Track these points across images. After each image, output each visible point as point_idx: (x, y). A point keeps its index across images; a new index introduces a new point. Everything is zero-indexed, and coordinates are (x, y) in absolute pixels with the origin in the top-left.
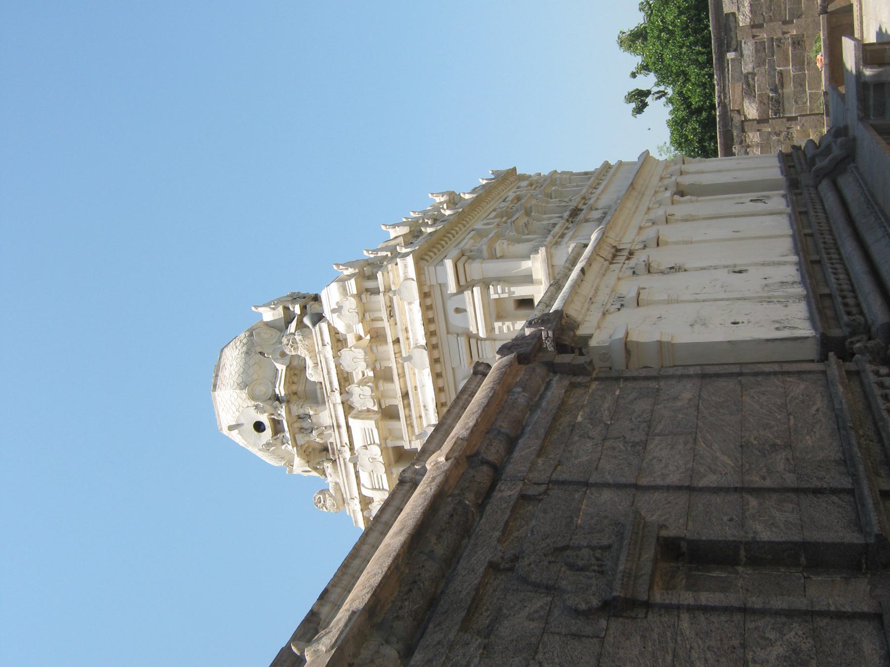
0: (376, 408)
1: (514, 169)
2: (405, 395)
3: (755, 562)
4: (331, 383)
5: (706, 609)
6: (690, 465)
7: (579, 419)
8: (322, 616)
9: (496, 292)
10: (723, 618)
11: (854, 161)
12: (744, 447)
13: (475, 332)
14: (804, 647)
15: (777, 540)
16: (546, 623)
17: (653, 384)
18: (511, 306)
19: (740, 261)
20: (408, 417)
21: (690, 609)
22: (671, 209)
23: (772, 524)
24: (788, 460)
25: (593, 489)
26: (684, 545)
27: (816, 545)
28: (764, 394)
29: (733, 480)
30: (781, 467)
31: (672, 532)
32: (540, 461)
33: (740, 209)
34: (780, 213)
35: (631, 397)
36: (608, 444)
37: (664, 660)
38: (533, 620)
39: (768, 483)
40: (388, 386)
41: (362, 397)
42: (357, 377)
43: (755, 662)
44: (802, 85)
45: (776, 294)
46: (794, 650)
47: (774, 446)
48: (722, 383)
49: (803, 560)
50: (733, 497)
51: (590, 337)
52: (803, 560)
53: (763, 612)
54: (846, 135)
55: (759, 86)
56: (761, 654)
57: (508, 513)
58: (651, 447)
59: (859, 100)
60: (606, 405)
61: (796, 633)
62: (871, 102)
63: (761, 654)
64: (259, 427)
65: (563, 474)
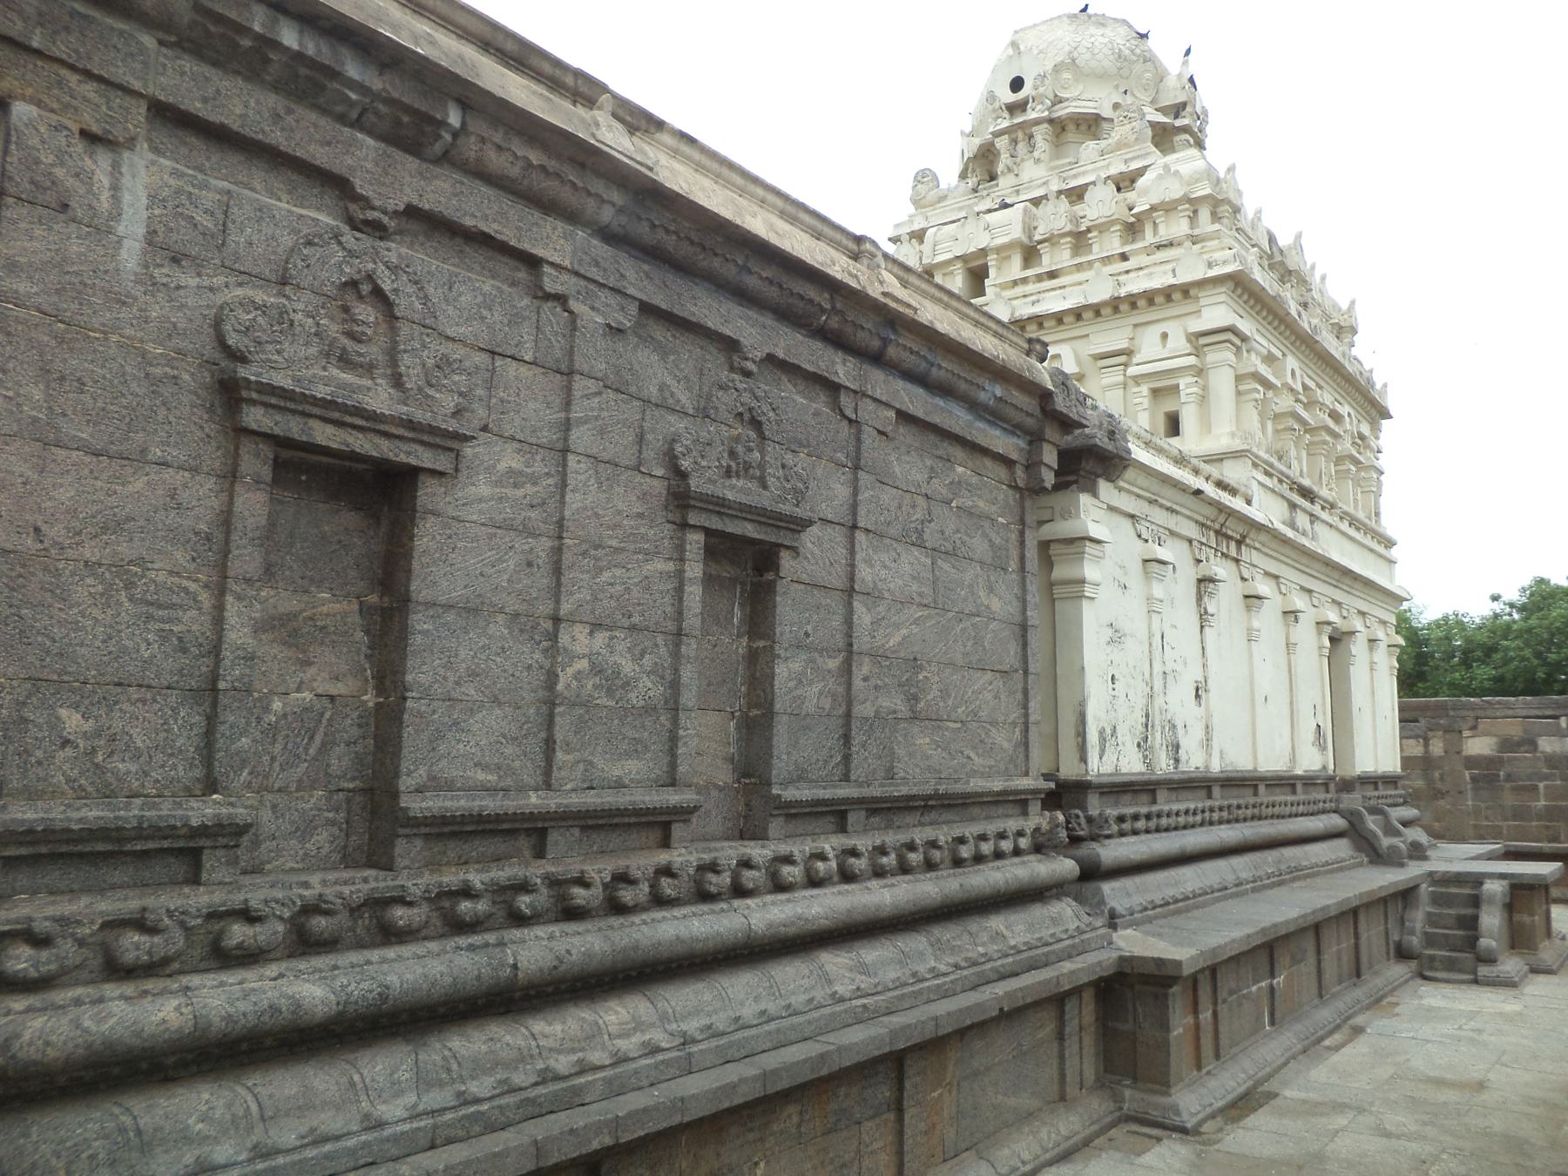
0: (1037, 237)
1: (1386, 414)
2: (1052, 275)
3: (752, 657)
4: (1075, 176)
5: (680, 590)
6: (886, 595)
7: (960, 469)
8: (658, 136)
9: (1188, 386)
10: (669, 609)
11: (1371, 862)
12: (914, 663)
13: (1135, 361)
14: (632, 695)
15: (776, 683)
16: (657, 405)
17: (1013, 565)
18: (1170, 406)
19: (1213, 698)
20: (1024, 281)
21: (680, 574)
22: (1382, 646)
23: (798, 680)
24: (895, 712)
25: (850, 476)
26: (770, 576)
27: (770, 727)
28: (996, 697)
29: (862, 642)
30: (886, 703)
31: (786, 561)
32: (892, 414)
33: (1304, 709)
34: (1293, 760)
35: (993, 536)
36: (921, 501)
37: (611, 537)
38: (661, 390)
39: (858, 683)
40: (1067, 254)
41: (1055, 218)
42: (1079, 209)
43: (611, 638)
44: (1515, 817)
45: (1158, 735)
46: (628, 683)
47: (916, 698)
48: (1013, 648)
49: (754, 712)
50: (840, 641)
51: (1095, 495)
52: (754, 712)
53: (676, 654)
54: (1411, 857)
55: (1516, 758)
56: (621, 647)
57: (811, 369)
58: (916, 552)
59: (1459, 874)
60: (981, 504)
61: (649, 688)
62: (1453, 890)
63: (621, 647)
64: (1017, 84)
65: (869, 438)
